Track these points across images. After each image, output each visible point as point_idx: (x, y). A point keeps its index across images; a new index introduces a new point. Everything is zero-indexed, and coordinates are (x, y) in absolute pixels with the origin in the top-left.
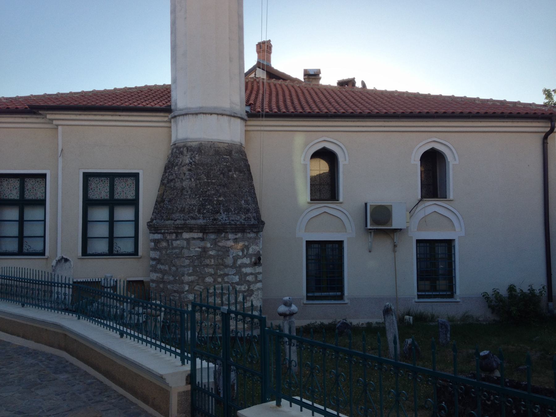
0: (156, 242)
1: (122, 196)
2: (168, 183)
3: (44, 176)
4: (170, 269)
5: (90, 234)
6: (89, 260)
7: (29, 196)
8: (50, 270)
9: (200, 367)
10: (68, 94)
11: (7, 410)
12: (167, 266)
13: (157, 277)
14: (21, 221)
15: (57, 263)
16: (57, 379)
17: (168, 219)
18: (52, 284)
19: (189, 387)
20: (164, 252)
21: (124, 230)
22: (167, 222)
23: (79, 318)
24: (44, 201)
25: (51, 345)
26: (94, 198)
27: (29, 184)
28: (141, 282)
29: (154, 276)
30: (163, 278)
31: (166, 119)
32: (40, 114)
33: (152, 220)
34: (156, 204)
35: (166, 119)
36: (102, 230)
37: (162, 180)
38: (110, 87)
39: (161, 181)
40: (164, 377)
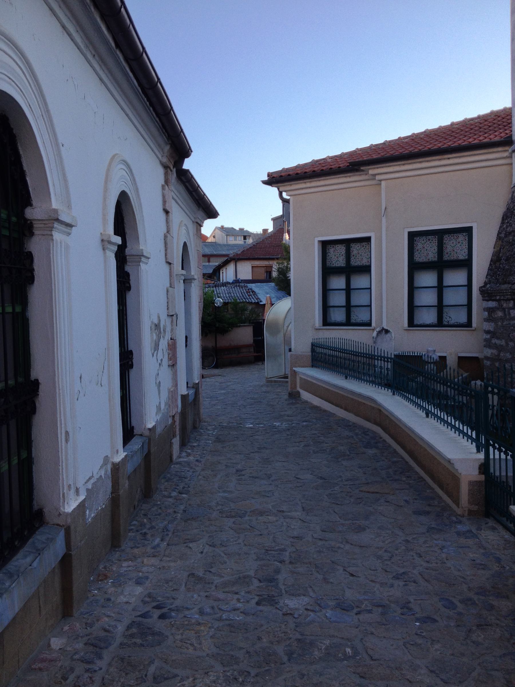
0: (490, 311)
1: (454, 257)
2: (506, 236)
3: (368, 240)
4: (507, 344)
5: (417, 303)
6: (417, 332)
7: (354, 262)
8: (370, 342)
9: (498, 457)
10: (396, 140)
11: (311, 474)
12: (503, 341)
13: (492, 353)
14: (348, 290)
15: (377, 334)
16: (365, 453)
17: (505, 283)
18: (372, 357)
19: (482, 478)
20: (500, 323)
21: (452, 297)
22: (503, 286)
23: (394, 394)
24: (370, 266)
25: (368, 420)
26: (421, 260)
27: (355, 249)
28: (476, 358)
29: (488, 352)
30: (499, 355)
31: (506, 154)
32: (363, 171)
33: (486, 284)
34: (490, 265)
35: (506, 154)
36: (427, 298)
37: (499, 233)
38: (446, 122)
39: (498, 235)
40: (451, 462)
